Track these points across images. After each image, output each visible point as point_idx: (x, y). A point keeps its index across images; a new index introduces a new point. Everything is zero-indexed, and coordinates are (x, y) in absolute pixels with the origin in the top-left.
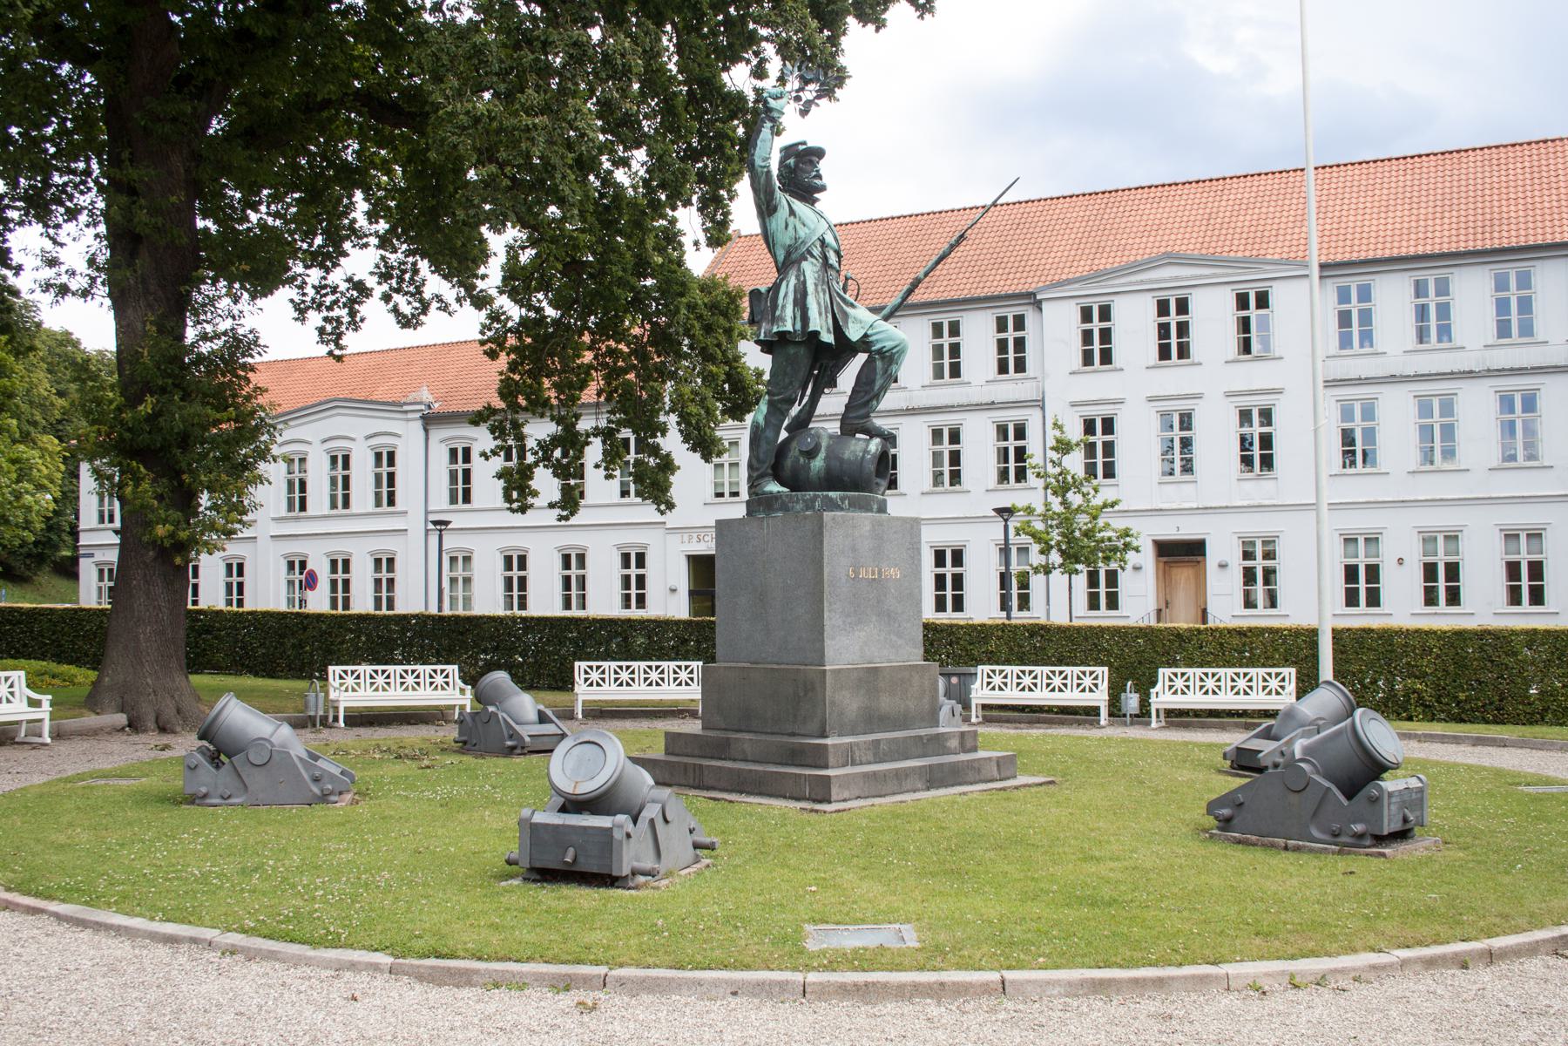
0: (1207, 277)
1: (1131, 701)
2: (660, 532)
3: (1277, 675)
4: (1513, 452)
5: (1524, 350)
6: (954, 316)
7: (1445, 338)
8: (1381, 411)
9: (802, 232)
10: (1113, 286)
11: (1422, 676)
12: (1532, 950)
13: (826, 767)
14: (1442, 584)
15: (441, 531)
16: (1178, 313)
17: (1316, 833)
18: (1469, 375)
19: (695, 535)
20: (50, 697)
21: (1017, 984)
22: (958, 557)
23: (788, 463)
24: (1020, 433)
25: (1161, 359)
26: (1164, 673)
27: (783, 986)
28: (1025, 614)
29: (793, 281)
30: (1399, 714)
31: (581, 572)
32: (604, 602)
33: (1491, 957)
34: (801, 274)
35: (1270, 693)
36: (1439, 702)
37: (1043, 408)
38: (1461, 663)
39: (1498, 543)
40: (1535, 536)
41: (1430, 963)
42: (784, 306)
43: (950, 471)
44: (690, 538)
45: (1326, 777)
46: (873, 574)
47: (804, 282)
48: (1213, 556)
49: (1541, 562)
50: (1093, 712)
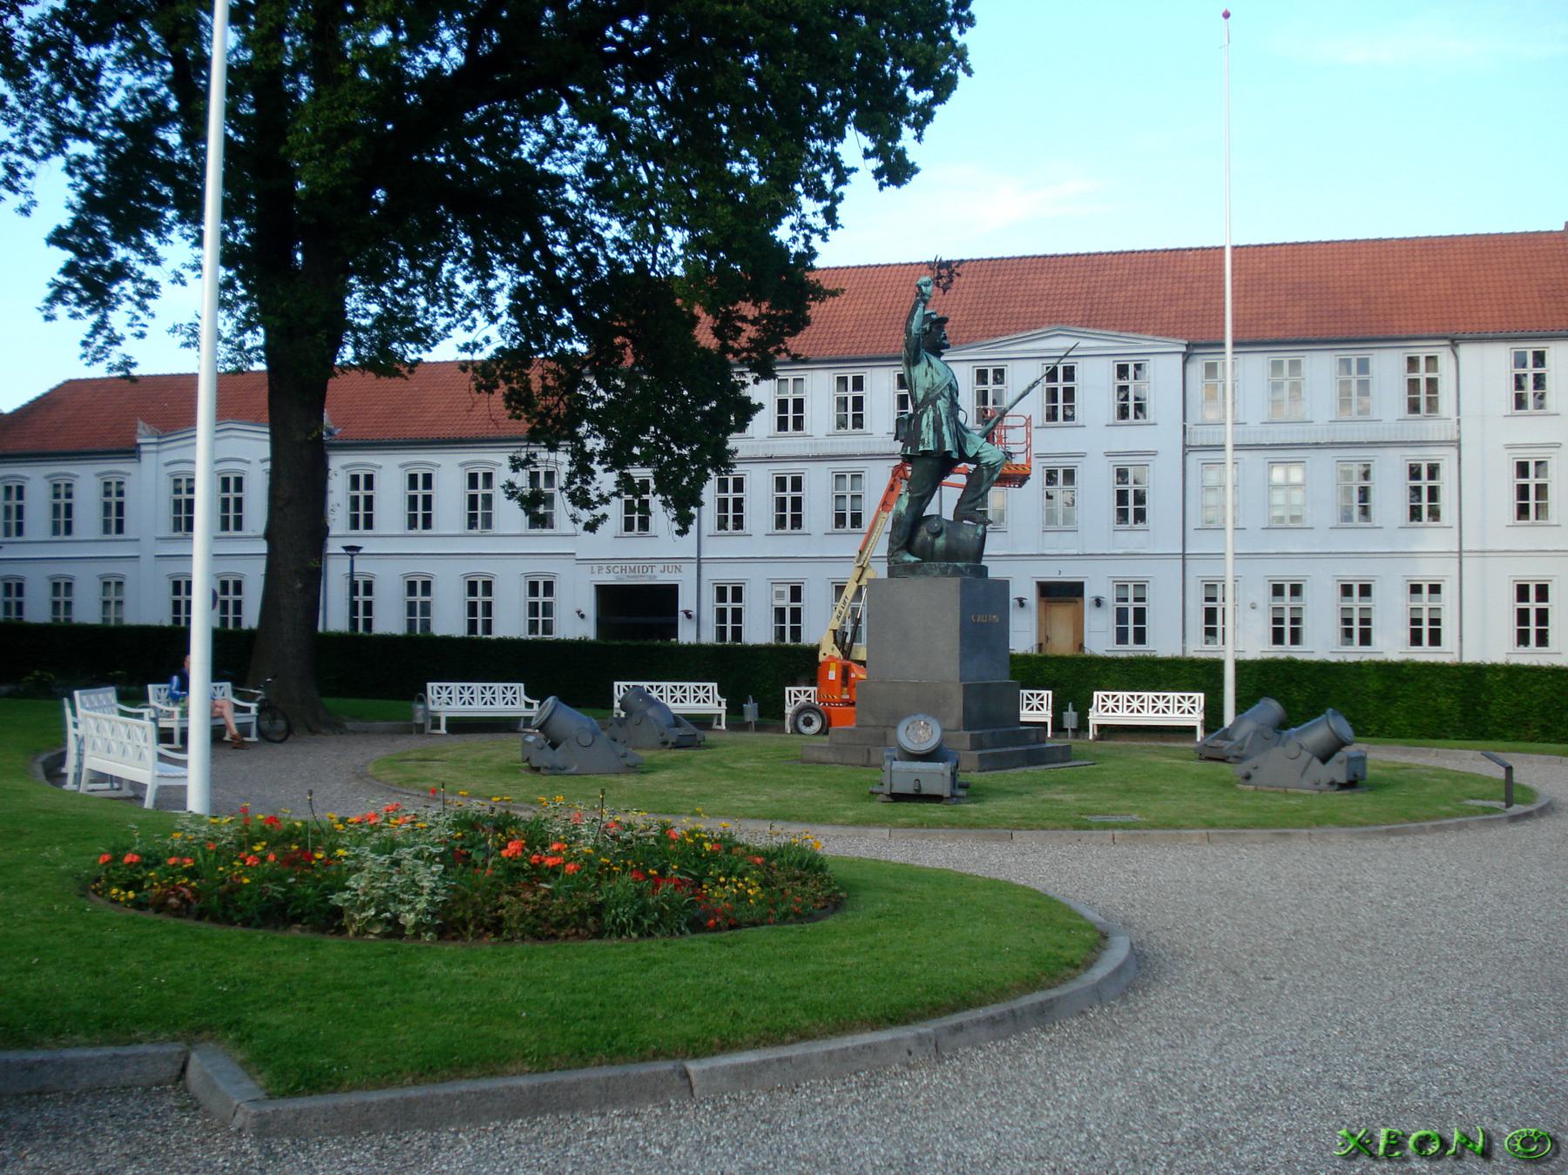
0: (1107, 348)
1: (1070, 719)
2: (570, 562)
3: (1038, 695)
5: (1362, 425)
6: (857, 372)
10: (1001, 353)
14: (1533, 627)
15: (352, 555)
16: (1535, 366)
18: (1317, 446)
19: (605, 566)
22: (738, 594)
24: (1433, 471)
25: (779, 430)
26: (1098, 695)
28: (1295, 648)
31: (487, 599)
32: (449, 621)
35: (1183, 712)
37: (1459, 448)
43: (790, 514)
44: (600, 569)
48: (1089, 594)
50: (1191, 730)
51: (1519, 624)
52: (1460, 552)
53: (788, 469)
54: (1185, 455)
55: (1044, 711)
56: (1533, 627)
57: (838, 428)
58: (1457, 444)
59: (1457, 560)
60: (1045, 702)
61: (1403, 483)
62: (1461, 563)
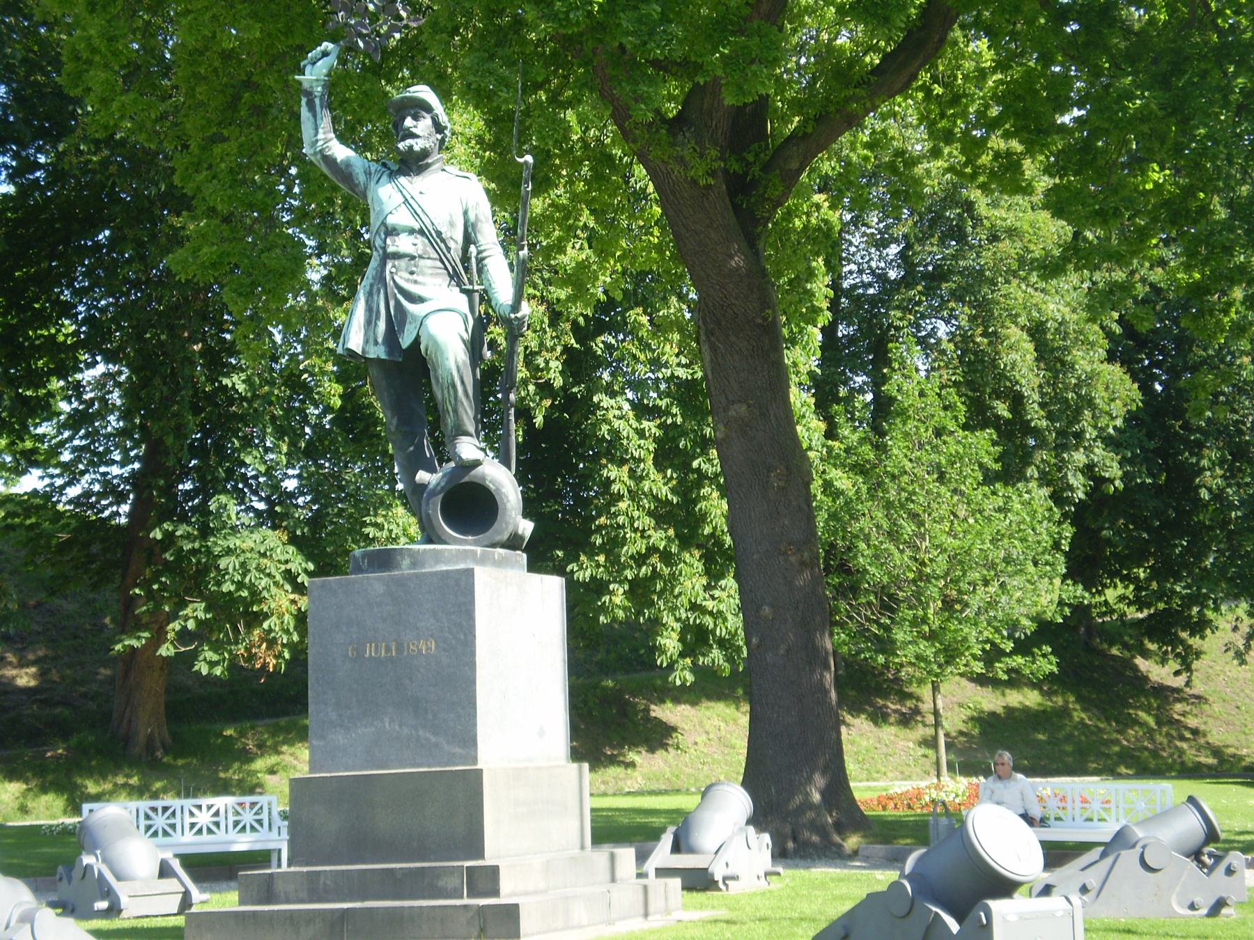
46: (388, 649)
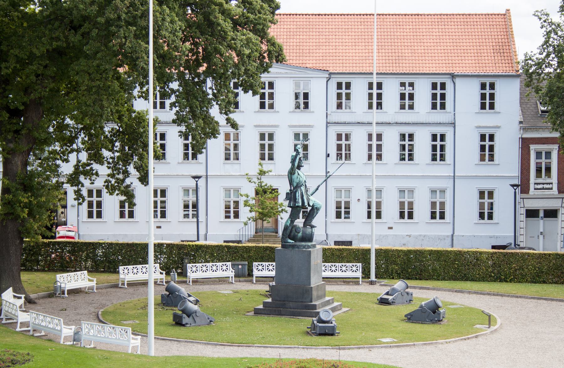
4: (404, 157)
7: (380, 108)
8: (353, 138)
9: (301, 179)
11: (397, 265)
12: (473, 337)
13: (316, 309)
17: (427, 320)
20: (24, 295)
21: (416, 344)
23: (292, 234)
24: (443, 137)
27: (388, 346)
29: (300, 192)
30: (390, 277)
33: (468, 338)
34: (301, 190)
36: (402, 272)
37: (455, 127)
38: (409, 260)
39: (397, 194)
40: (411, 191)
41: (461, 339)
42: (298, 199)
45: (429, 309)
47: (302, 192)
49: (413, 202)
51: (89, 208)
52: (454, 176)
53: (407, 130)
54: (327, 127)
55: (358, 272)
56: (95, 209)
57: (296, 108)
58: (453, 124)
59: (453, 180)
60: (358, 268)
61: (429, 143)
62: (454, 181)
